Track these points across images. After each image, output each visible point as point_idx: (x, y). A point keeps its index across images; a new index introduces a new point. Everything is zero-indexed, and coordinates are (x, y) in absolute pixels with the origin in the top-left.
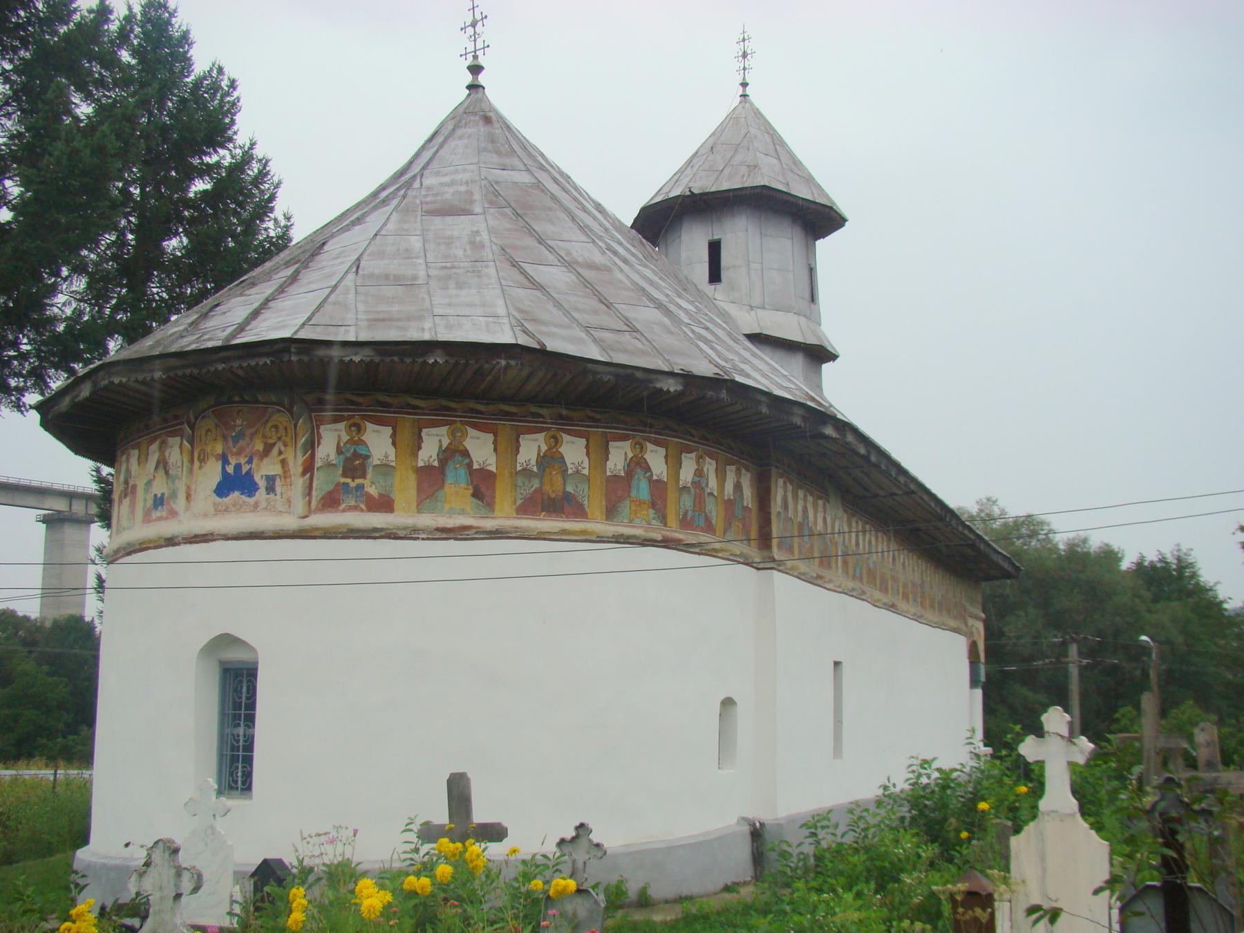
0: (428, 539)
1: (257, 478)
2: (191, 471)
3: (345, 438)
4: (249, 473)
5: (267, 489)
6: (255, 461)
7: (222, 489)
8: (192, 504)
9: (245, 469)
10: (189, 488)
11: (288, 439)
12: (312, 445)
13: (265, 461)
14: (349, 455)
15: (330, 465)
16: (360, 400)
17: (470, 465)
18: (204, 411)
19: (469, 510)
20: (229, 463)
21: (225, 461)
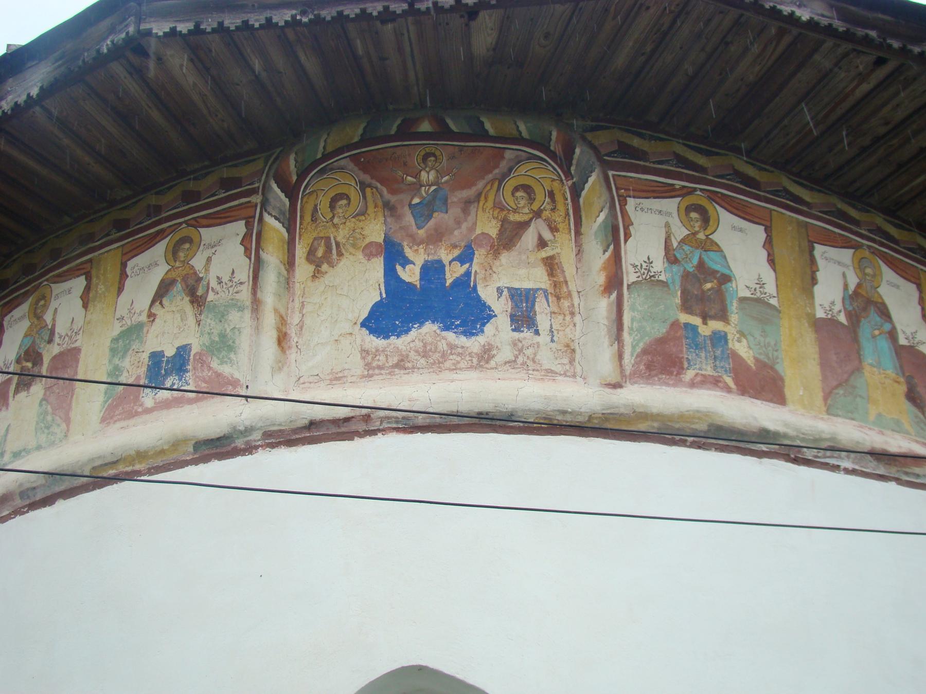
0: (853, 472)
1: (487, 294)
2: (288, 284)
3: (680, 232)
4: (464, 282)
5: (513, 318)
6: (480, 256)
7: (381, 321)
8: (292, 355)
9: (454, 272)
10: (282, 321)
11: (558, 217)
12: (615, 235)
13: (505, 257)
14: (690, 268)
15: (651, 281)
16: (701, 160)
17: (892, 335)
18: (326, 157)
19: (907, 426)
20: (406, 262)
21: (392, 254)
